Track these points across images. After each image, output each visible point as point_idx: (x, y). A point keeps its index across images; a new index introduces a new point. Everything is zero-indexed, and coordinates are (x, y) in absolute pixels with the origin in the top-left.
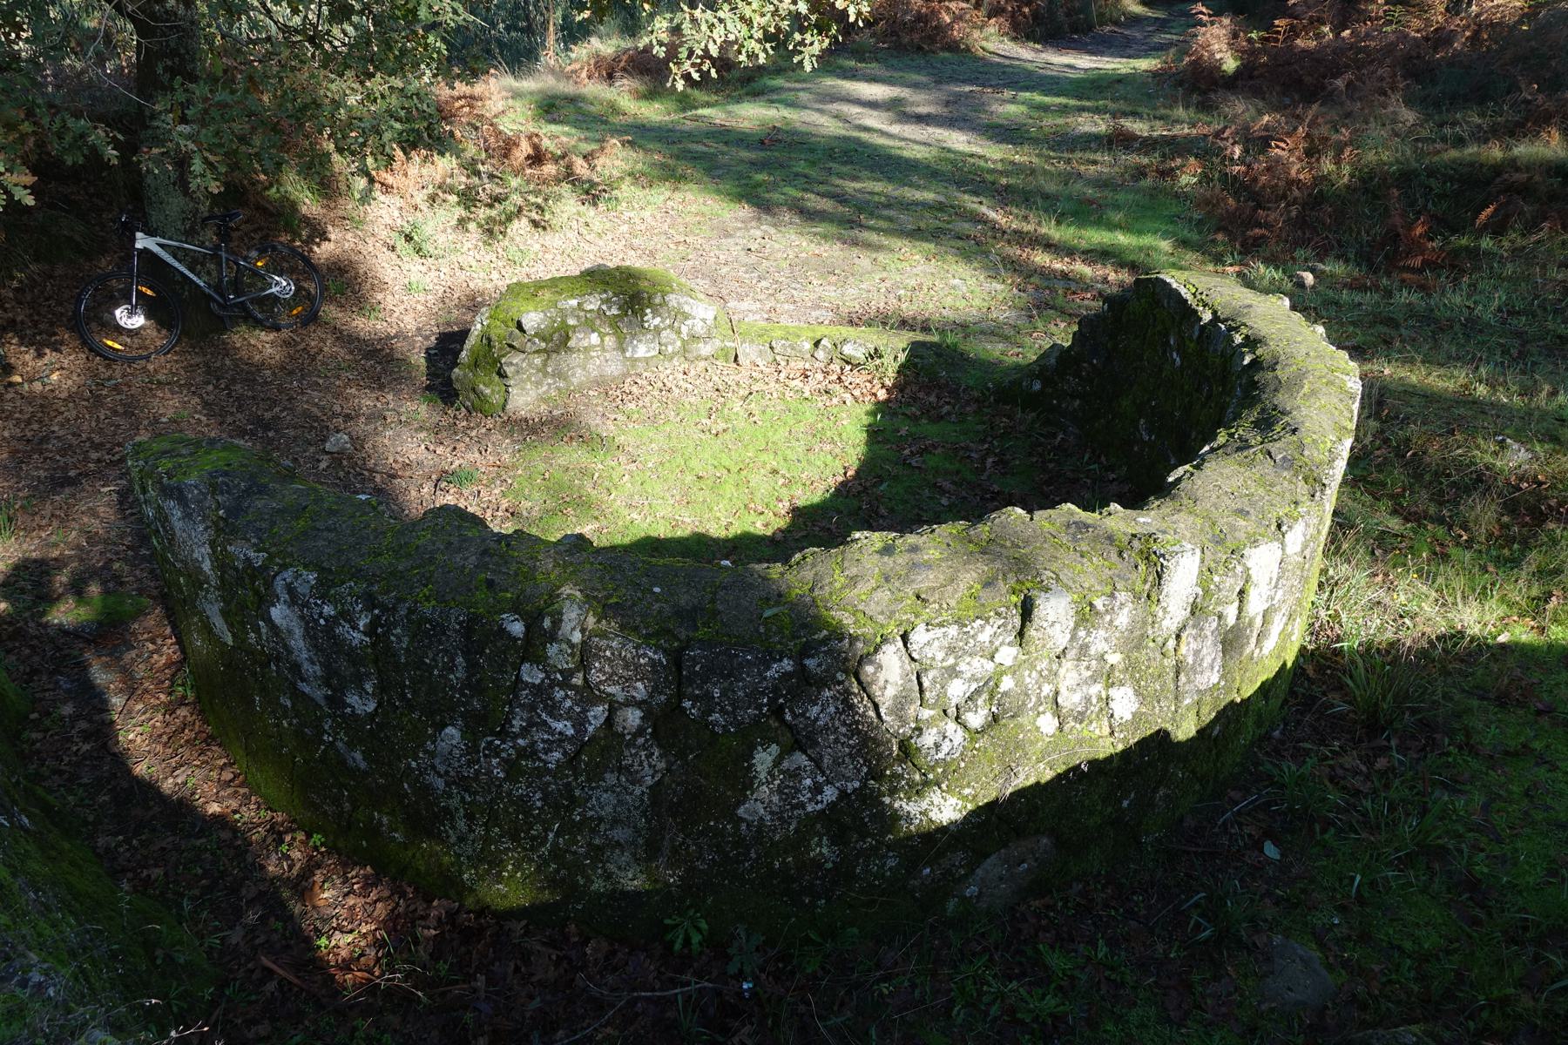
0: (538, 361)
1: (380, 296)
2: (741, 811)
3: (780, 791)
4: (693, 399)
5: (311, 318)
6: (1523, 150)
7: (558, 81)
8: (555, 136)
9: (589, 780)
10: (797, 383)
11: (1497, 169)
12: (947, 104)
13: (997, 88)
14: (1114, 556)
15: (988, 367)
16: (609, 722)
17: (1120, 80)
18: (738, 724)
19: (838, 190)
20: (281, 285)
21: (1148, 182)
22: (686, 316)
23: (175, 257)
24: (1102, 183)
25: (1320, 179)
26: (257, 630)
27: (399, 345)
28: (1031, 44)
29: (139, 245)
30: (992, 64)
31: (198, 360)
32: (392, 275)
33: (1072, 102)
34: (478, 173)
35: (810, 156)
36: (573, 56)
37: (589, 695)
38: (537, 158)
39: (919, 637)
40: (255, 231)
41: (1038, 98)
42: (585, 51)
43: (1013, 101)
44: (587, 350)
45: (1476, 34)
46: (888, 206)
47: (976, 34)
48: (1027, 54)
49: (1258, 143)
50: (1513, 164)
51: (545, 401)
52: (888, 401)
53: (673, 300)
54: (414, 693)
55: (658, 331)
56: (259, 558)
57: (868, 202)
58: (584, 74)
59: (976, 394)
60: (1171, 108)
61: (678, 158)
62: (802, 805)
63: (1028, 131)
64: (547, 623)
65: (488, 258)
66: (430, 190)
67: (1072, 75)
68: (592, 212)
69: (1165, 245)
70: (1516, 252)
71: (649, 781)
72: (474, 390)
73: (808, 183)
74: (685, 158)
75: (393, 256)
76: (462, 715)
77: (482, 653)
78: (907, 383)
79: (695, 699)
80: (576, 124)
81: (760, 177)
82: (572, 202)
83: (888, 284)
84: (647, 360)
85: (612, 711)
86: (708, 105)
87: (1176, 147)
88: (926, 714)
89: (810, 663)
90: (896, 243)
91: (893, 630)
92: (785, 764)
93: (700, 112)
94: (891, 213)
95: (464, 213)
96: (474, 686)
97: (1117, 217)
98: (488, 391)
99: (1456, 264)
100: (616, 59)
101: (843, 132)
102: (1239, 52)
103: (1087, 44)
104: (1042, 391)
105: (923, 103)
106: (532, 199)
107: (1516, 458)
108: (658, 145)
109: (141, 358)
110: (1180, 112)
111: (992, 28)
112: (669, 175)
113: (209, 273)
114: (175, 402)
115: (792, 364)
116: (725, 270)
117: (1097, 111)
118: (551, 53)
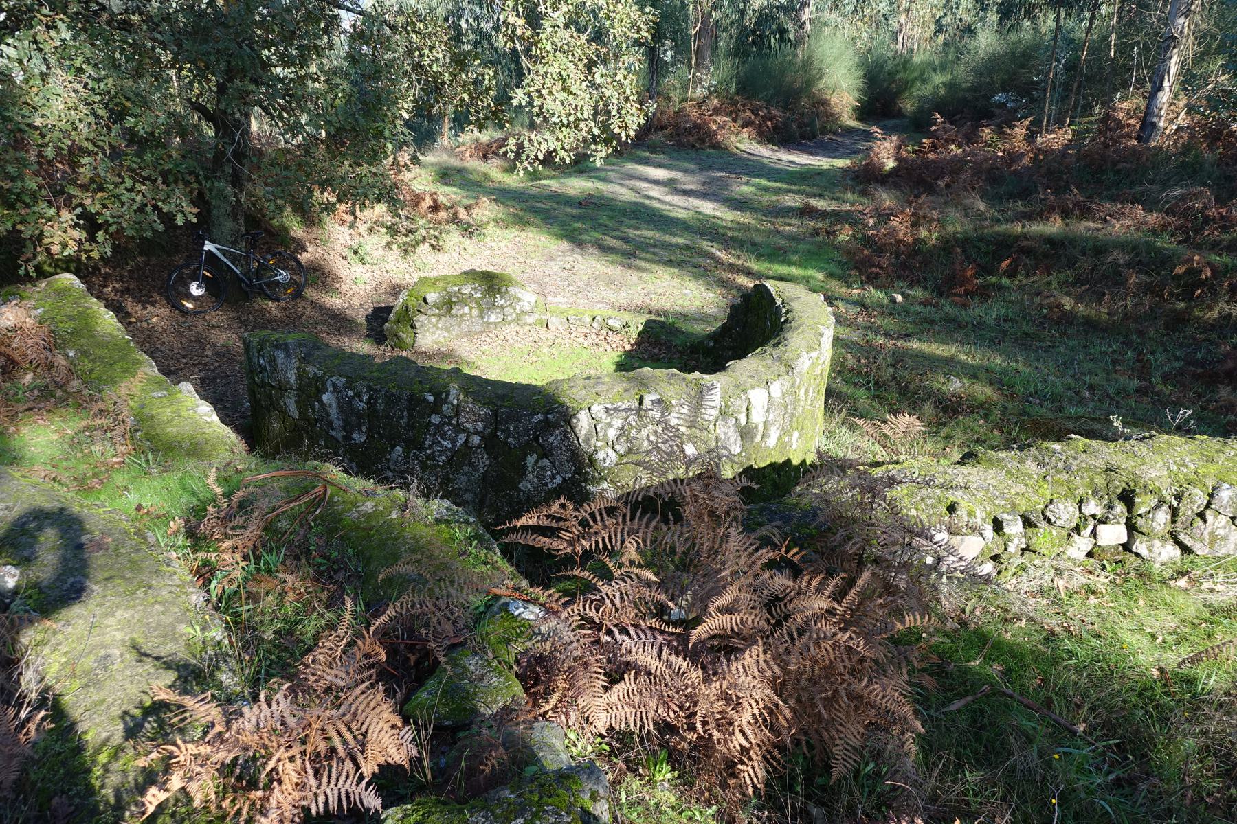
0: (434, 320)
1: (338, 285)
2: (520, 486)
3: (537, 477)
4: (520, 346)
5: (298, 295)
6: (1037, 228)
7: (450, 156)
8: (448, 193)
9: (456, 470)
10: (581, 340)
11: (1017, 238)
12: (704, 184)
13: (739, 174)
14: (684, 385)
15: (688, 334)
16: (466, 442)
17: (820, 173)
18: (520, 443)
19: (625, 235)
20: (283, 275)
21: (820, 238)
22: (520, 300)
23: (224, 255)
24: (792, 238)
25: (918, 241)
26: (313, 408)
27: (350, 312)
28: (771, 146)
29: (206, 248)
30: (741, 159)
31: (234, 315)
32: (345, 273)
33: (785, 186)
34: (398, 216)
35: (610, 213)
36: (460, 140)
37: (459, 428)
38: (435, 208)
39: (595, 408)
40: (263, 244)
41: (764, 182)
42: (468, 137)
43: (747, 184)
44: (462, 316)
45: (1036, 156)
46: (655, 246)
47: (733, 138)
48: (766, 152)
49: (883, 216)
50: (1024, 236)
51: (436, 343)
52: (631, 350)
53: (512, 290)
54: (384, 429)
55: (503, 307)
56: (320, 373)
57: (642, 243)
58: (467, 154)
59: (680, 349)
60: (844, 193)
61: (525, 211)
62: (546, 484)
63: (752, 204)
64: (443, 396)
65: (403, 266)
66: (369, 224)
67: (792, 168)
68: (467, 242)
69: (820, 276)
70: (1021, 287)
71: (482, 470)
72: (396, 335)
73: (607, 230)
74: (530, 211)
75: (346, 263)
76: (404, 440)
77: (415, 410)
78: (642, 342)
79: (502, 431)
80: (460, 187)
81: (577, 225)
82: (456, 235)
83: (646, 291)
84: (496, 324)
85: (468, 437)
86: (549, 178)
87: (839, 217)
88: (599, 444)
89: (550, 416)
90: (655, 267)
91: (585, 406)
92: (540, 464)
93: (542, 182)
94: (656, 250)
95: (390, 239)
96: (411, 426)
97: (795, 258)
98: (404, 336)
99: (984, 293)
100: (489, 145)
101: (634, 199)
102: (898, 159)
103: (810, 147)
104: (714, 347)
105: (689, 182)
106: (432, 232)
107: (956, 385)
108: (513, 203)
109: (201, 312)
110: (849, 196)
111: (745, 134)
112: (520, 221)
113: (242, 266)
114: (224, 336)
115: (579, 330)
116: (548, 279)
117: (798, 192)
118: (445, 137)
